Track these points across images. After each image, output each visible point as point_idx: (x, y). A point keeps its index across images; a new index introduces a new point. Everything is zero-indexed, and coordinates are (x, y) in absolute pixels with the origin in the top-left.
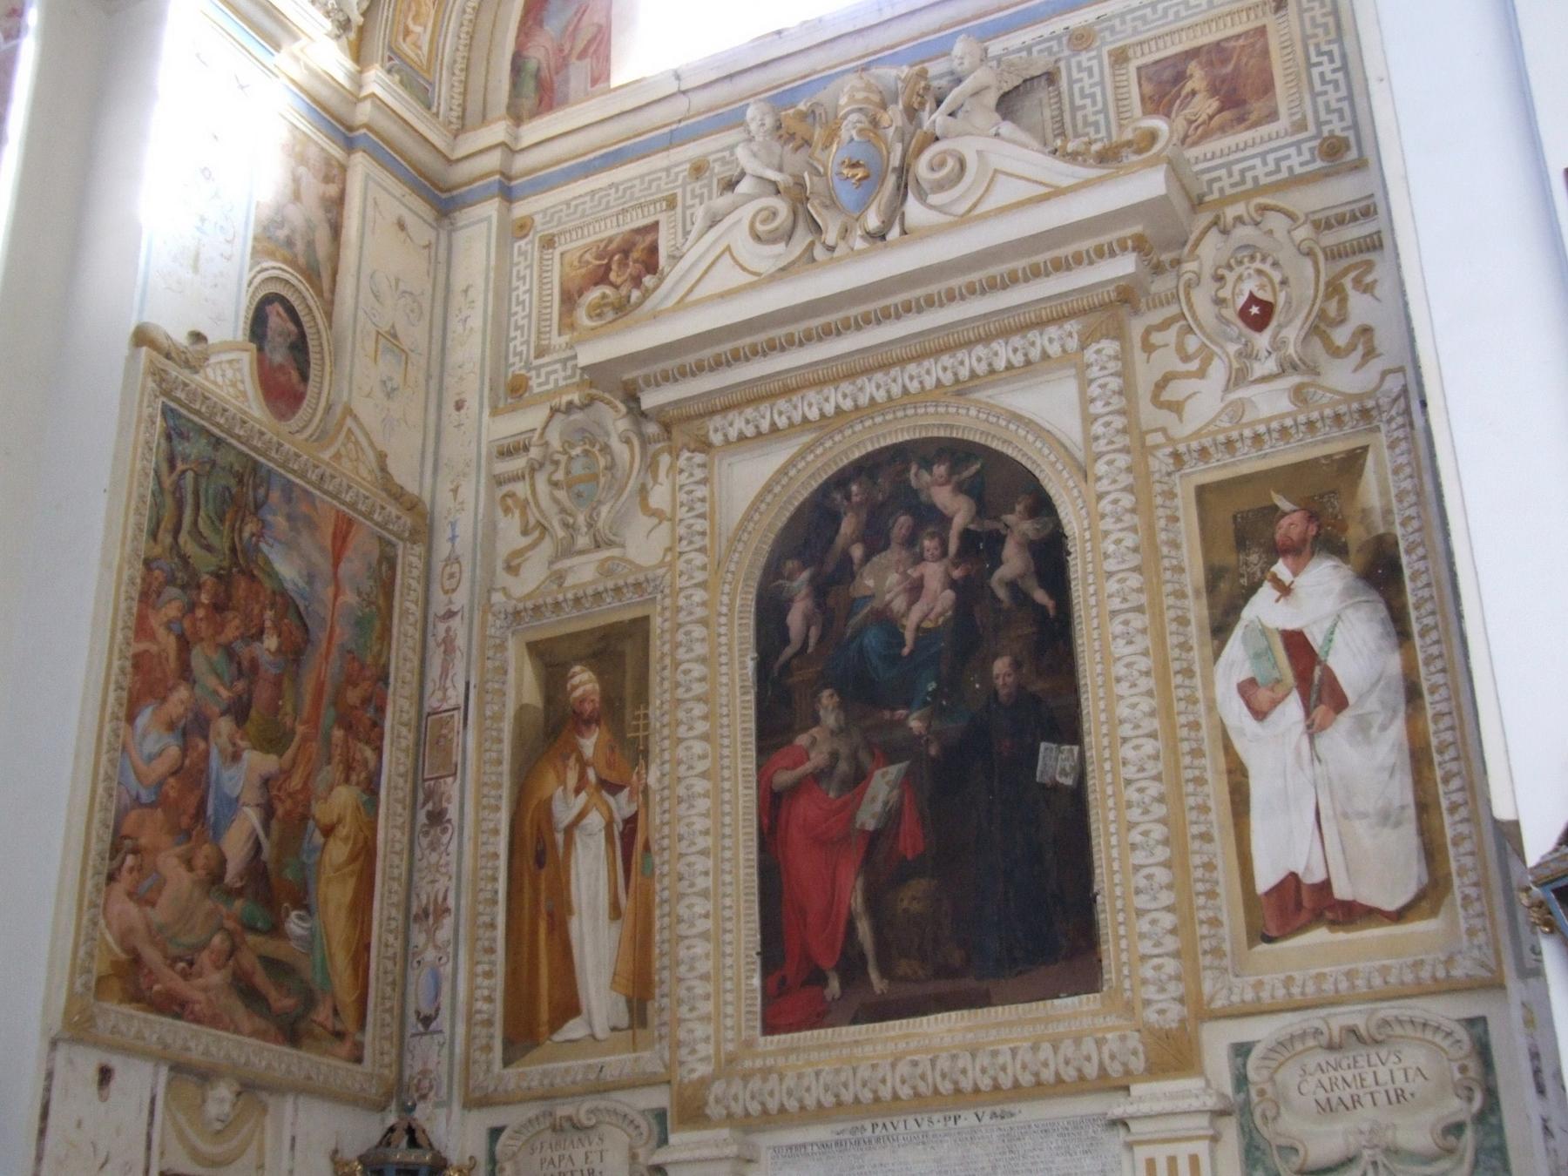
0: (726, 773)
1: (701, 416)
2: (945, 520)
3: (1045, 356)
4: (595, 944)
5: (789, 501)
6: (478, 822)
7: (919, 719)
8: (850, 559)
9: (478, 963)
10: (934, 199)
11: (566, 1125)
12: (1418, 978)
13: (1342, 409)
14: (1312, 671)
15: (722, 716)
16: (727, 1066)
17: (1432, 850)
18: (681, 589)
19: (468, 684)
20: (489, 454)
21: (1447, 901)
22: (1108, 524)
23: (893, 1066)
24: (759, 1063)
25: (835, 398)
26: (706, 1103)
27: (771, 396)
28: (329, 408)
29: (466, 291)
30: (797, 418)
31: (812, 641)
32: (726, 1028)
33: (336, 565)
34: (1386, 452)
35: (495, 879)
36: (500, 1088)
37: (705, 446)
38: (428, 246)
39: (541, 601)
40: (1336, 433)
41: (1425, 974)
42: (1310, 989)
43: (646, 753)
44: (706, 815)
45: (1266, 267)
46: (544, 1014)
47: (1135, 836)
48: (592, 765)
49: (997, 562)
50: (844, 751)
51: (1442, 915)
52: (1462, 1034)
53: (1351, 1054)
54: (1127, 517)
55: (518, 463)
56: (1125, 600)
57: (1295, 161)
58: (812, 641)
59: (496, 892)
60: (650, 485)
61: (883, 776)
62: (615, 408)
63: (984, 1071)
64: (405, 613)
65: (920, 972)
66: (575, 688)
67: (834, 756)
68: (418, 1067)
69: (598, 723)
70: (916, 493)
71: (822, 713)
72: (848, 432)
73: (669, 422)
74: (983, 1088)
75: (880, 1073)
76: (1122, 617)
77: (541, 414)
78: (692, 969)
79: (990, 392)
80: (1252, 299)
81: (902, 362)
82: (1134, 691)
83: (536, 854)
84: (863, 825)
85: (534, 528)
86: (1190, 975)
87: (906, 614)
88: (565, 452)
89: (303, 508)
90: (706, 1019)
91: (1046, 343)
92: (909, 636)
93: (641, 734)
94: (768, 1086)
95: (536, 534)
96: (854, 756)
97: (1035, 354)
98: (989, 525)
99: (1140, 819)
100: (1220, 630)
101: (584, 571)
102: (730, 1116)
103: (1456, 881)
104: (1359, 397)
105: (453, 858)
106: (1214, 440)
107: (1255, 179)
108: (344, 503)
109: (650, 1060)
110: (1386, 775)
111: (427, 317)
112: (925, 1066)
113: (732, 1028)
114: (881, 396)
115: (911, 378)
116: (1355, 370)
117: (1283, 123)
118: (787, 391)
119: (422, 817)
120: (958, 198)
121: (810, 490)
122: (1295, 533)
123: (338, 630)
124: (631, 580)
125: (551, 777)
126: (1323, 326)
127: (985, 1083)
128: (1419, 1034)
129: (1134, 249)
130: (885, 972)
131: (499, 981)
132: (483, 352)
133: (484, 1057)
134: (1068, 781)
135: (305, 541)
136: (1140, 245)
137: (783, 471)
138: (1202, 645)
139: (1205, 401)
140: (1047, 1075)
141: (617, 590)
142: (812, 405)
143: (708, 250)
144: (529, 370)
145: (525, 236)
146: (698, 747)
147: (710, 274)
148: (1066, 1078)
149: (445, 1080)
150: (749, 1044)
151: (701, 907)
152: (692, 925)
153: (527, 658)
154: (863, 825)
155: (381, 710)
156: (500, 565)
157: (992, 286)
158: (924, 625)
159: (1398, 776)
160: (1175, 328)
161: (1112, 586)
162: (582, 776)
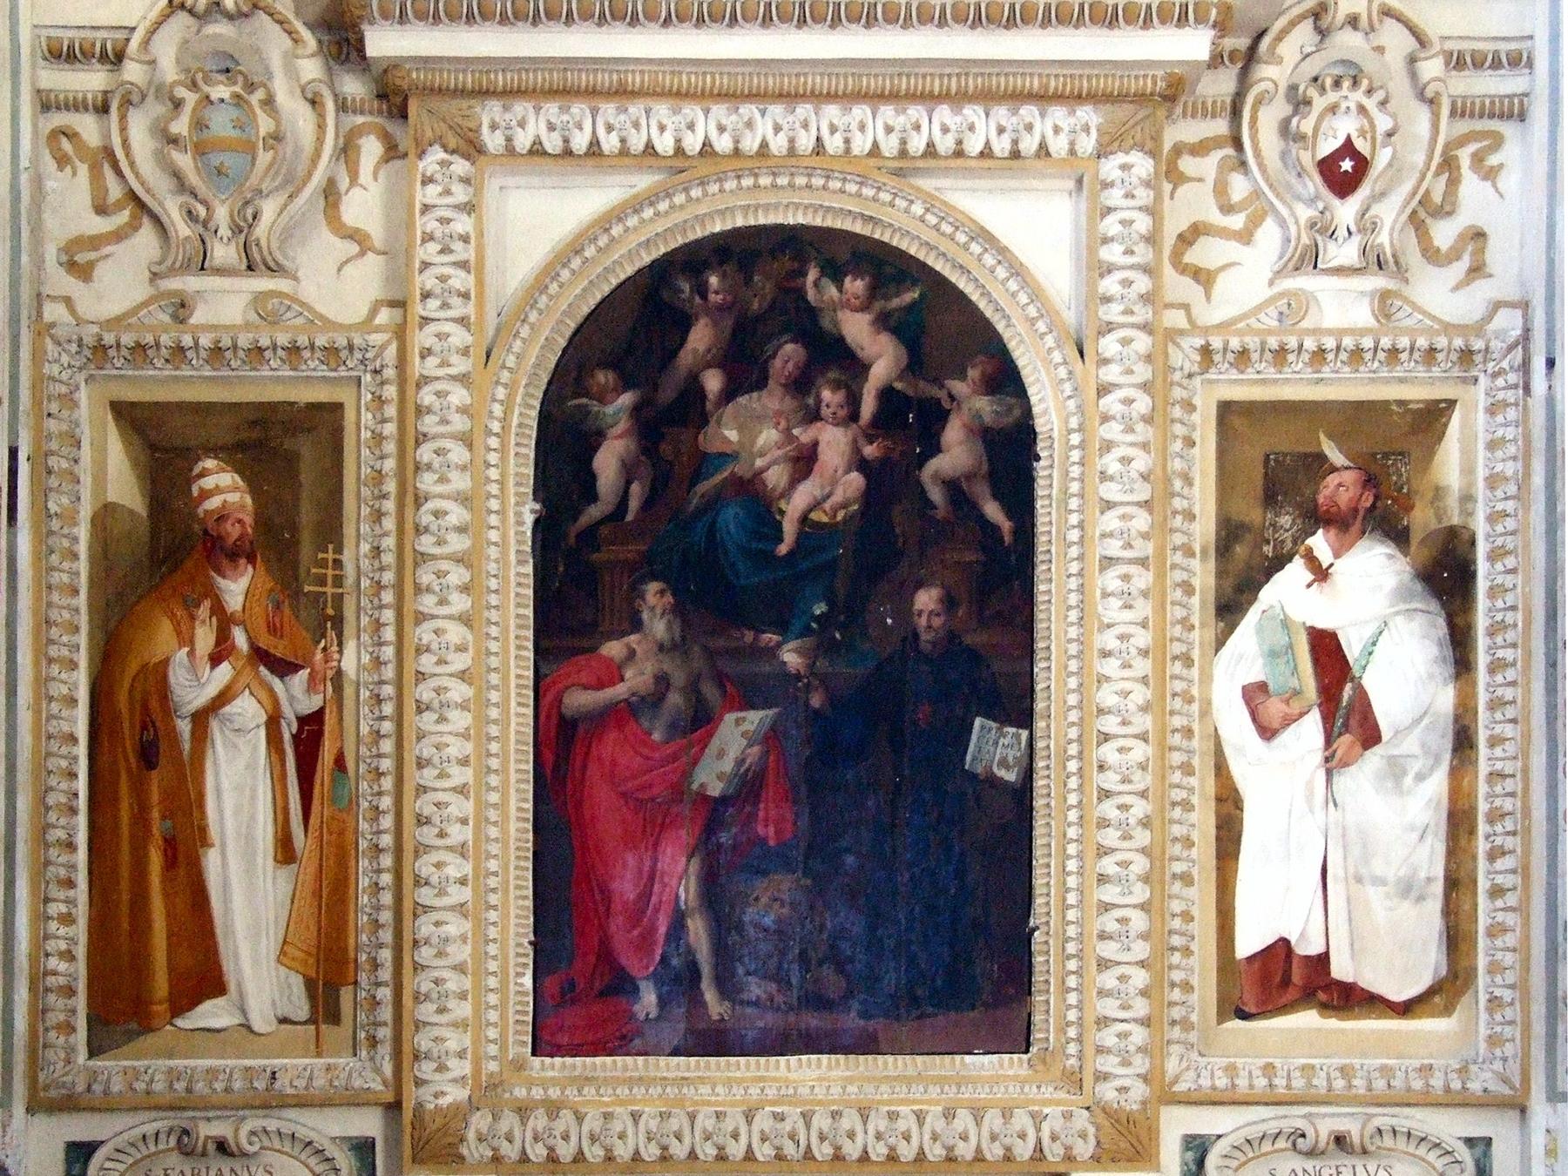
1: (461, 92)
3: (1043, 151)
4: (250, 898)
7: (795, 650)
8: (701, 393)
11: (211, 1147)
13: (1441, 342)
14: (1342, 689)
16: (487, 1093)
17: (1456, 938)
21: (1466, 999)
22: (1112, 431)
23: (749, 1117)
25: (705, 126)
30: (637, 143)
31: (634, 504)
34: (1481, 417)
35: (73, 775)
37: (472, 148)
39: (149, 339)
41: (1437, 1082)
42: (1298, 1083)
44: (465, 736)
45: (1371, 104)
46: (161, 985)
47: (1108, 865)
48: (242, 623)
49: (934, 448)
50: (679, 678)
51: (1456, 1015)
52: (1464, 1154)
53: (1333, 1163)
54: (1140, 427)
55: (92, 80)
58: (634, 504)
60: (344, 182)
61: (738, 722)
66: (206, 494)
67: (662, 681)
69: (251, 559)
70: (812, 312)
71: (645, 616)
72: (713, 188)
74: (874, 1157)
76: (1122, 569)
78: (441, 954)
80: (1348, 148)
81: (820, 97)
82: (1127, 673)
85: (119, 207)
88: (194, 86)
91: (1049, 133)
92: (789, 528)
94: (560, 1126)
95: (124, 216)
97: (1029, 145)
99: (1116, 844)
101: (225, 304)
103: (1482, 979)
104: (1462, 329)
106: (1263, 344)
110: (1415, 836)
112: (794, 1120)
114: (778, 144)
115: (833, 129)
116: (1456, 288)
118: (622, 93)
122: (1344, 498)
124: (321, 341)
125: (165, 629)
126: (1422, 214)
131: (80, 930)
133: (62, 1039)
134: (1010, 776)
138: (1203, 625)
139: (1246, 279)
141: (294, 350)
142: (664, 127)
148: (988, 1157)
150: (519, 1065)
151: (456, 868)
152: (442, 893)
156: (51, 253)
158: (814, 516)
159: (1429, 839)
160: (1216, 156)
161: (1111, 521)
162: (223, 637)
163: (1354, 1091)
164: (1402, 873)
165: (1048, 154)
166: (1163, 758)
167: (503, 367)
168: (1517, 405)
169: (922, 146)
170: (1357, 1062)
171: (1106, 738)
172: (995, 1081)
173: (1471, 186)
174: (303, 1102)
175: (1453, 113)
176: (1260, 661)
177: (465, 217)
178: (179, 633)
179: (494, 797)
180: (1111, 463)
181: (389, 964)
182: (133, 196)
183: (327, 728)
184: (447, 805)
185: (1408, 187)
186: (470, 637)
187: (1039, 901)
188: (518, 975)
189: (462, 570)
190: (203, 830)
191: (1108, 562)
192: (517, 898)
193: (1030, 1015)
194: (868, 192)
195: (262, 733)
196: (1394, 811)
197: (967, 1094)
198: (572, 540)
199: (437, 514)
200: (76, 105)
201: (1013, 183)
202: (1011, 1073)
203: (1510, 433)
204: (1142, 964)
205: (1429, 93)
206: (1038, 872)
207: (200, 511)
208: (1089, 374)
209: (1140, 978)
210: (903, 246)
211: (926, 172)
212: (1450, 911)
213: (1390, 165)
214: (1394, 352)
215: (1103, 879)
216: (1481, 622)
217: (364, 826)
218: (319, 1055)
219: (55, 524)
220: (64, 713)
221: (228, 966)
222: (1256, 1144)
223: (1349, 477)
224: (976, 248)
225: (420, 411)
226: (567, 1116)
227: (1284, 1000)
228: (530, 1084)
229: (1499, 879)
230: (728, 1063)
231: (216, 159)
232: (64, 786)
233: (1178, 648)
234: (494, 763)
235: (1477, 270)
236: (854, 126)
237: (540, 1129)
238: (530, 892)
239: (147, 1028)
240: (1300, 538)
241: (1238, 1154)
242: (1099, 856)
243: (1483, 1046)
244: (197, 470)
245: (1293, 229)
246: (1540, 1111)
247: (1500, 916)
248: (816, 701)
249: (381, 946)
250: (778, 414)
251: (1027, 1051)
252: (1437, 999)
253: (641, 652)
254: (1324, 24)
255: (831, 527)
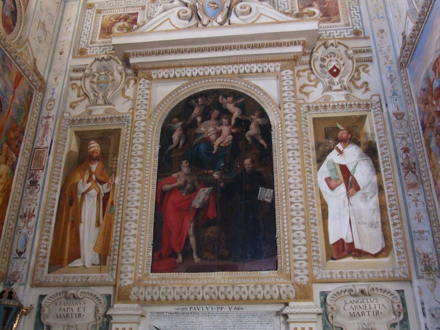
0: (147, 182)
1: (149, 69)
2: (229, 114)
3: (269, 71)
4: (89, 235)
5: (176, 100)
6: (50, 187)
9: (43, 235)
10: (240, 17)
11: (72, 297)
12: (384, 276)
13: (361, 103)
14: (349, 178)
15: (147, 163)
16: (138, 282)
17: (386, 237)
18: (136, 121)
19: (52, 141)
20: (70, 70)
21: (391, 252)
22: (288, 123)
23: (203, 288)
24: (150, 282)
25: (197, 71)
26: (130, 294)
27: (175, 67)
28: (21, 37)
29: (68, 20)
30: (183, 75)
32: (139, 269)
33: (15, 88)
34: (373, 118)
35: (53, 207)
36: (47, 281)
37: (150, 78)
38: (58, 3)
39: (83, 118)
40: (358, 110)
41: (386, 275)
43: (115, 173)
44: (139, 195)
45: (338, 59)
46: (66, 256)
47: (294, 220)
48: (95, 174)
49: (248, 129)
50: (189, 181)
52: (397, 294)
53: (361, 298)
54: (294, 122)
55: (80, 74)
56: (293, 146)
57: (346, 34)
59: (53, 212)
60: (126, 88)
61: (203, 191)
62: (118, 63)
63: (237, 293)
64: (33, 113)
65: (212, 257)
66: (91, 148)
67: (186, 182)
68: (14, 270)
69: (98, 160)
70: (221, 104)
71: (182, 168)
72: (200, 82)
73: (136, 71)
75: (198, 290)
76: (292, 151)
77: (93, 60)
79: (250, 79)
80: (335, 67)
82: (295, 174)
83: (70, 201)
84: (194, 205)
86: (310, 268)
87: (215, 140)
88: (98, 73)
89: (8, 65)
90: (132, 264)
92: (215, 148)
93: (114, 166)
94: (155, 291)
96: (193, 184)
97: (266, 70)
98: (245, 118)
100: (320, 161)
101: (99, 111)
102: (138, 300)
103: (395, 247)
104: (366, 101)
105: (39, 198)
107: (333, 36)
108: (21, 69)
109: (108, 277)
110: (372, 212)
111: (54, 23)
113: (141, 269)
114: (213, 73)
115: (224, 69)
116: (363, 93)
117: (342, 23)
118: (181, 66)
119: (28, 183)
120: (250, 18)
121: (184, 98)
122: (344, 136)
123: (11, 111)
124: (117, 116)
125: (79, 175)
126: (353, 80)
127: (237, 297)
128: (382, 294)
129: (302, 45)
130: (199, 256)
131: (50, 243)
132: (72, 39)
133: (41, 269)
134: (269, 201)
135: (6, 76)
136: (304, 44)
137: (176, 90)
139: (316, 94)
140: (260, 296)
141: (111, 118)
142: (189, 72)
143: (161, 18)
144: (88, 47)
145: (91, 9)
146: (138, 172)
147: (162, 25)
148: (266, 298)
149: (25, 276)
150: (147, 275)
151: (134, 226)
152: (130, 231)
153: (74, 136)
154: (194, 205)
155: (20, 142)
156: (68, 105)
157: (253, 47)
159: (376, 212)
160: (307, 72)
161: (289, 141)
162: (90, 177)
163: (365, 278)
164: (370, 221)
165: (270, 71)
166: (306, 195)
167: (153, 118)
168: (380, 114)
169: (243, 72)
170: (364, 270)
171: (291, 190)
172: (268, 278)
173: (363, 74)
174: (94, 285)
175: (357, 61)
176: (328, 172)
177: (147, 90)
178: (81, 176)
179: (145, 209)
180: (288, 129)
181: (117, 250)
182: (85, 94)
183: (110, 196)
184: (133, 211)
185: (349, 74)
186: (141, 173)
187: (278, 231)
188: (148, 252)
189: (141, 159)
190: (80, 219)
191: (289, 150)
192: (149, 233)
193: (277, 260)
194: (232, 81)
195: (96, 197)
196: (366, 206)
197: (260, 281)
198: (167, 153)
199: (136, 147)
200: (78, 79)
201: (264, 78)
202: (272, 275)
203: (380, 120)
204: (304, 245)
205: (351, 57)
206: (277, 224)
207: (89, 152)
208: (282, 112)
209: (304, 249)
210: (241, 91)
211: (244, 77)
212: (384, 230)
213: (344, 70)
214: (351, 105)
215: (293, 224)
216: (380, 161)
217: (116, 217)
218: (100, 273)
219: (58, 154)
220: (54, 194)
221: (82, 251)
222: (340, 294)
223: (345, 132)
224: (256, 90)
225: (135, 127)
226: (157, 288)
227: (343, 255)
228: (149, 279)
229: (395, 221)
230: (199, 274)
231: (100, 85)
232: (51, 209)
233: (308, 169)
234: (145, 201)
235: (367, 89)
236: (228, 68)
237: (149, 291)
238: (153, 232)
239: (62, 267)
240: (334, 145)
241: (335, 297)
242: (292, 218)
243: (397, 265)
244: (90, 143)
245: (325, 83)
246: (416, 282)
247: (397, 230)
248: (222, 185)
249: (116, 245)
250: (213, 124)
251: (277, 270)
252: (383, 253)
253: (181, 176)
254: (326, 46)
255: (225, 147)
